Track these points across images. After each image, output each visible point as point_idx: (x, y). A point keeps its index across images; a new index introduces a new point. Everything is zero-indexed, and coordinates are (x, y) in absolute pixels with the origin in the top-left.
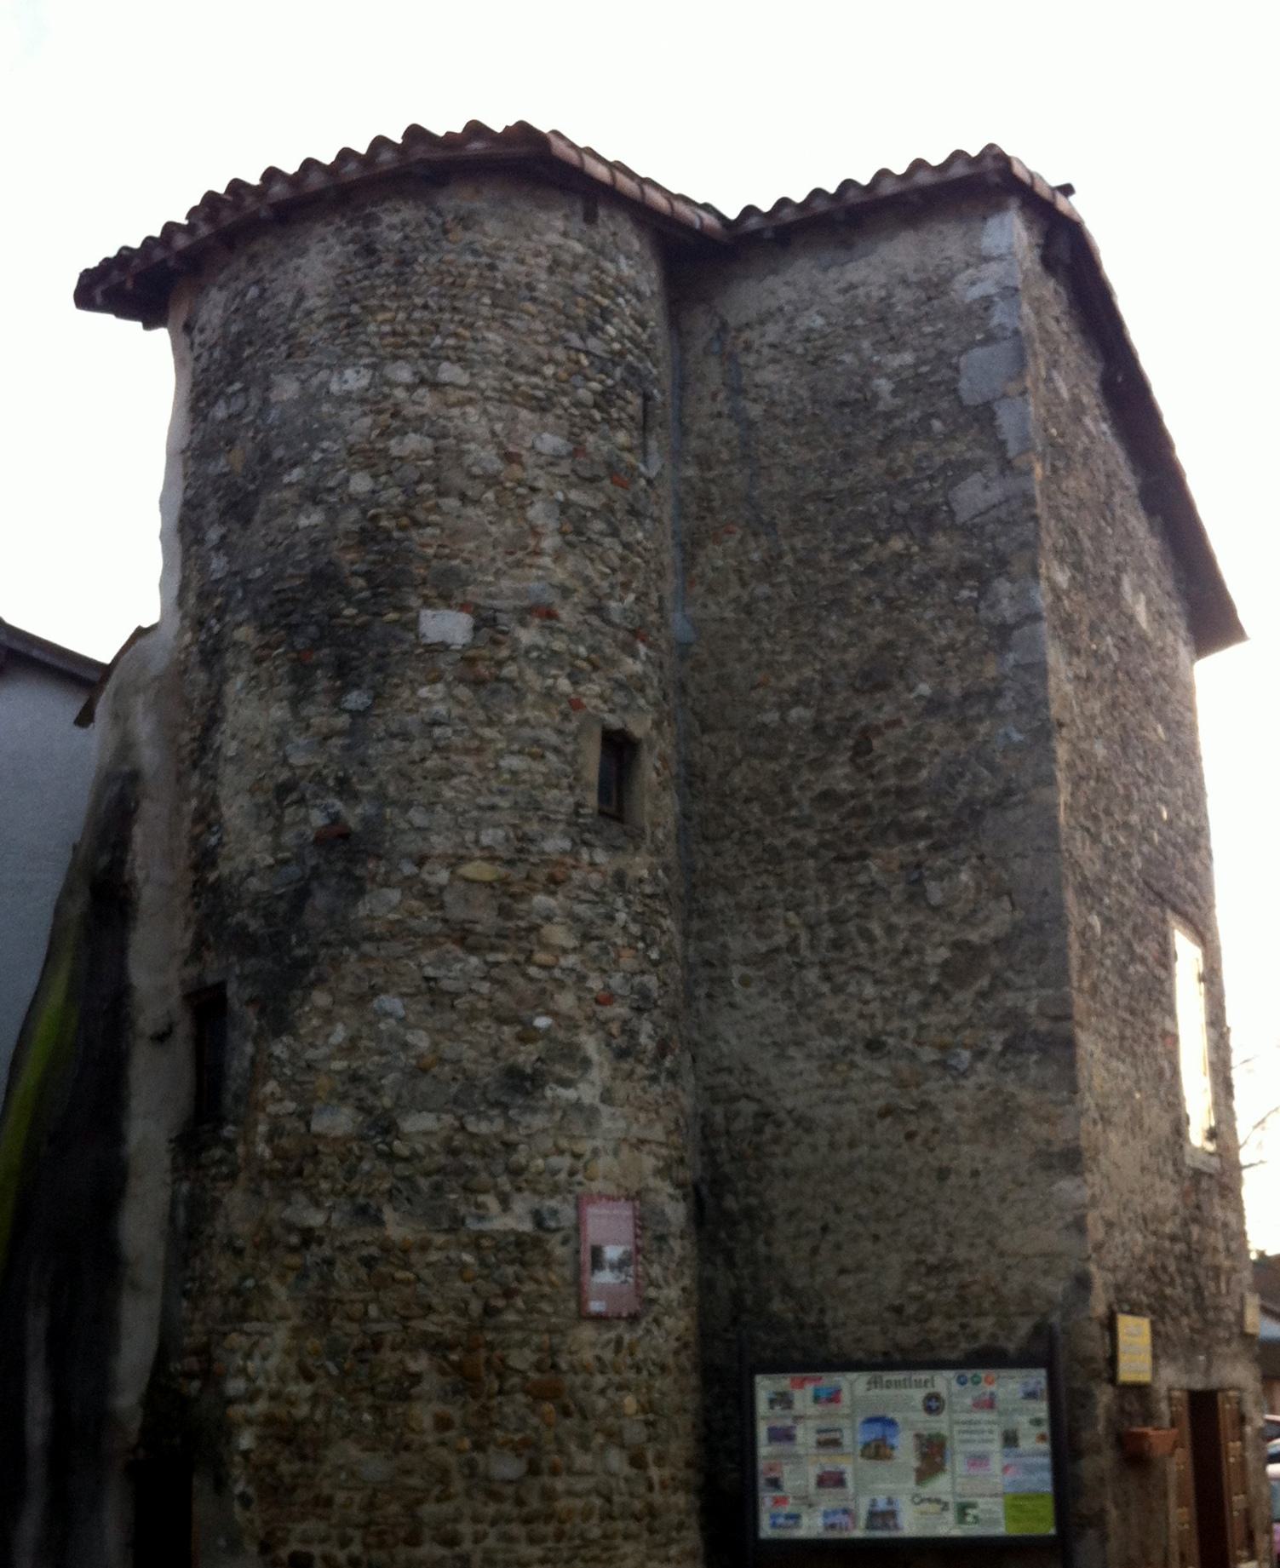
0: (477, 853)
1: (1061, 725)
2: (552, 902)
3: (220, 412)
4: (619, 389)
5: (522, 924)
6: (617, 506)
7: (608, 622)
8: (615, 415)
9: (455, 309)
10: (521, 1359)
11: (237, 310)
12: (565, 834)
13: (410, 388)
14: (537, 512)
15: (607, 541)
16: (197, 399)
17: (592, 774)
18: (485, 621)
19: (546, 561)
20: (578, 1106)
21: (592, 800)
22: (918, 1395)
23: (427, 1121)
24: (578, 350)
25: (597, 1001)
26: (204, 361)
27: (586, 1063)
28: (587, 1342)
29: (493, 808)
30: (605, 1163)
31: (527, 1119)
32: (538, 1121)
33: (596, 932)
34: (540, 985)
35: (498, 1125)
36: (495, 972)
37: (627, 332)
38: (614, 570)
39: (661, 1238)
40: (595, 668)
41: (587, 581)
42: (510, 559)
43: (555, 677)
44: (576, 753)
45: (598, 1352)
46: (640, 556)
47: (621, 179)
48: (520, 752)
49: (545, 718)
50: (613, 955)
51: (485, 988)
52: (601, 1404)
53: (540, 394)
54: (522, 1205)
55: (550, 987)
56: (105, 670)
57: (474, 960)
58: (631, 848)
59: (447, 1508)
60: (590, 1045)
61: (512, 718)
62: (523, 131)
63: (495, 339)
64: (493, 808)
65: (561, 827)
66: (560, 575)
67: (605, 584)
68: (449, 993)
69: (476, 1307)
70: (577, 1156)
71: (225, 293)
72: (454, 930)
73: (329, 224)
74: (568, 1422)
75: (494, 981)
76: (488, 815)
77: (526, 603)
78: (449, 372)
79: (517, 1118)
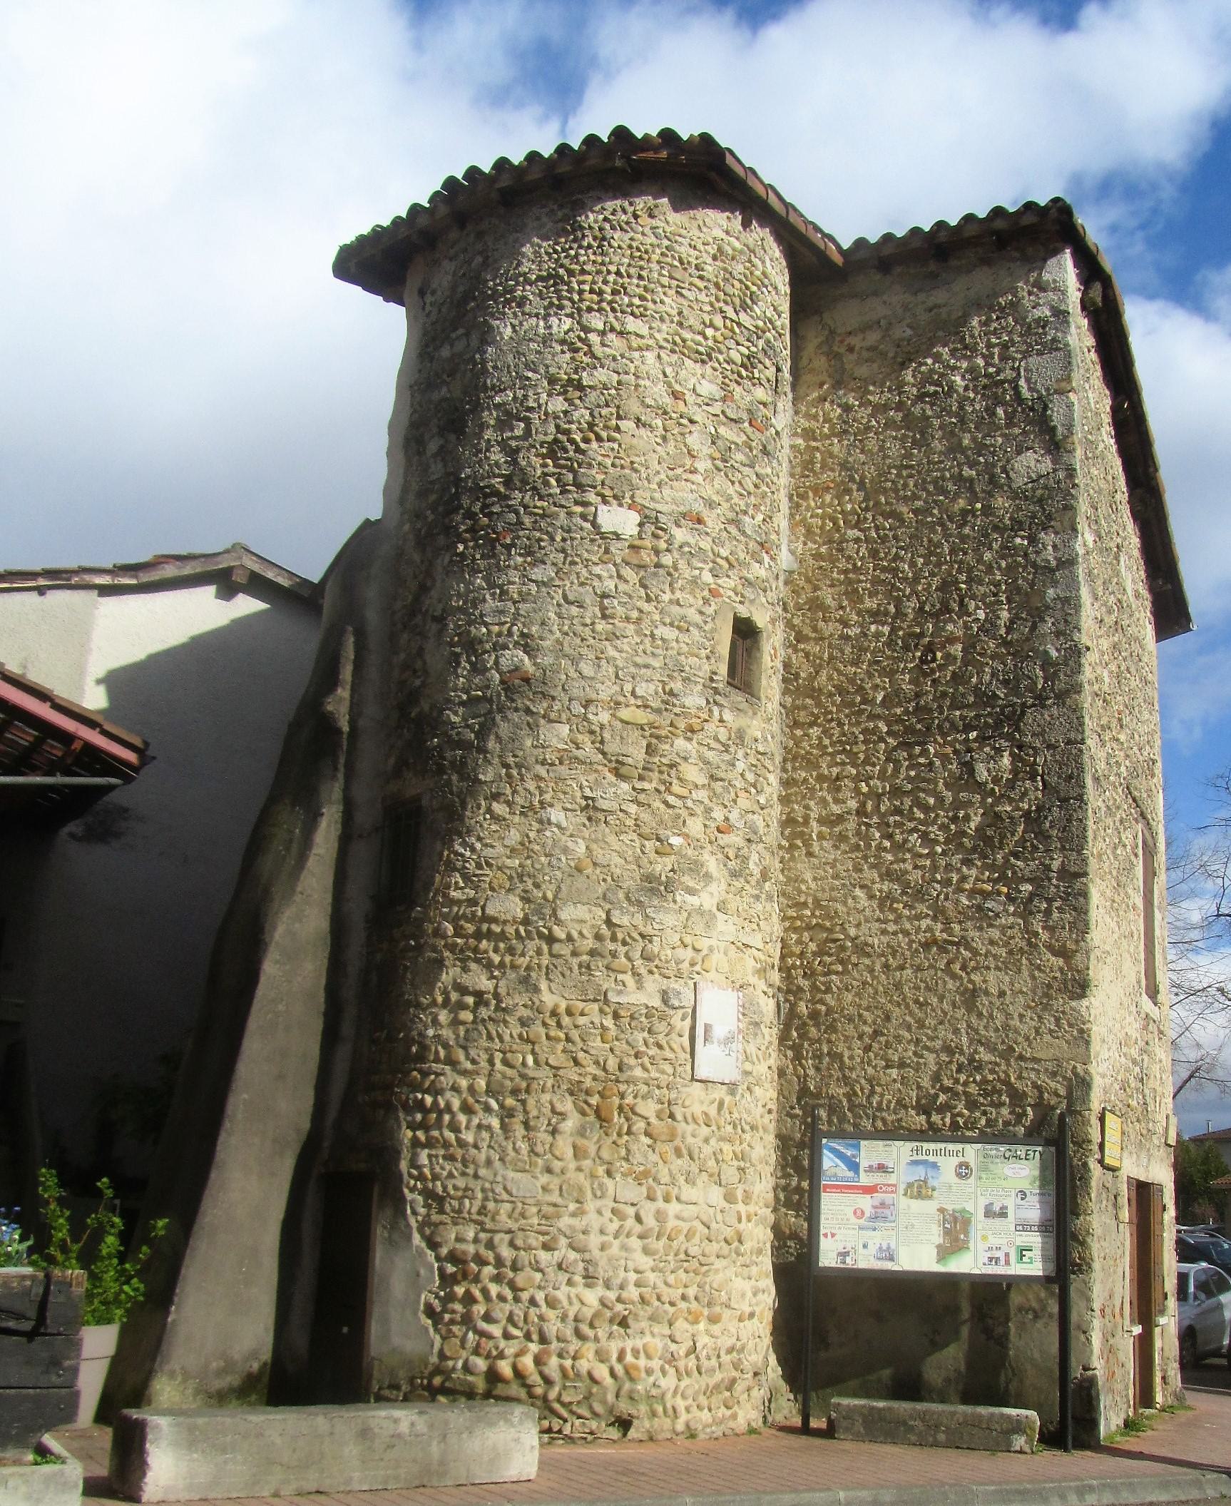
0: (632, 701)
1: (1088, 649)
2: (688, 746)
3: (445, 352)
4: (760, 356)
5: (665, 761)
6: (754, 444)
7: (744, 533)
8: (757, 375)
9: (640, 277)
10: (648, 1108)
11: (464, 274)
12: (702, 694)
13: (602, 333)
14: (694, 441)
15: (746, 470)
16: (427, 346)
17: (724, 649)
18: (649, 519)
19: (698, 478)
20: (700, 911)
21: (723, 669)
22: (955, 1161)
23: (581, 912)
24: (733, 321)
25: (719, 831)
26: (434, 317)
27: (708, 877)
28: (696, 1100)
29: (647, 666)
30: (716, 958)
31: (659, 916)
32: (669, 920)
33: (722, 775)
34: (677, 811)
35: (638, 919)
36: (642, 797)
37: (768, 314)
38: (749, 493)
39: (757, 1024)
40: (731, 566)
41: (729, 499)
42: (670, 473)
43: (701, 569)
44: (714, 630)
45: (705, 1108)
46: (768, 486)
47: (772, 196)
48: (671, 625)
49: (692, 600)
50: (733, 794)
51: (633, 809)
52: (707, 1150)
53: (701, 349)
54: (653, 984)
55: (684, 813)
56: (318, 589)
57: (625, 786)
58: (750, 713)
59: (577, 1223)
60: (712, 864)
61: (666, 597)
62: (706, 140)
63: (670, 304)
64: (647, 666)
65: (700, 687)
66: (709, 492)
67: (742, 503)
68: (604, 811)
69: (612, 1063)
70: (697, 950)
71: (454, 263)
72: (610, 761)
73: (544, 206)
74: (679, 1162)
75: (639, 804)
76: (643, 671)
77: (682, 509)
78: (632, 324)
79: (652, 915)
